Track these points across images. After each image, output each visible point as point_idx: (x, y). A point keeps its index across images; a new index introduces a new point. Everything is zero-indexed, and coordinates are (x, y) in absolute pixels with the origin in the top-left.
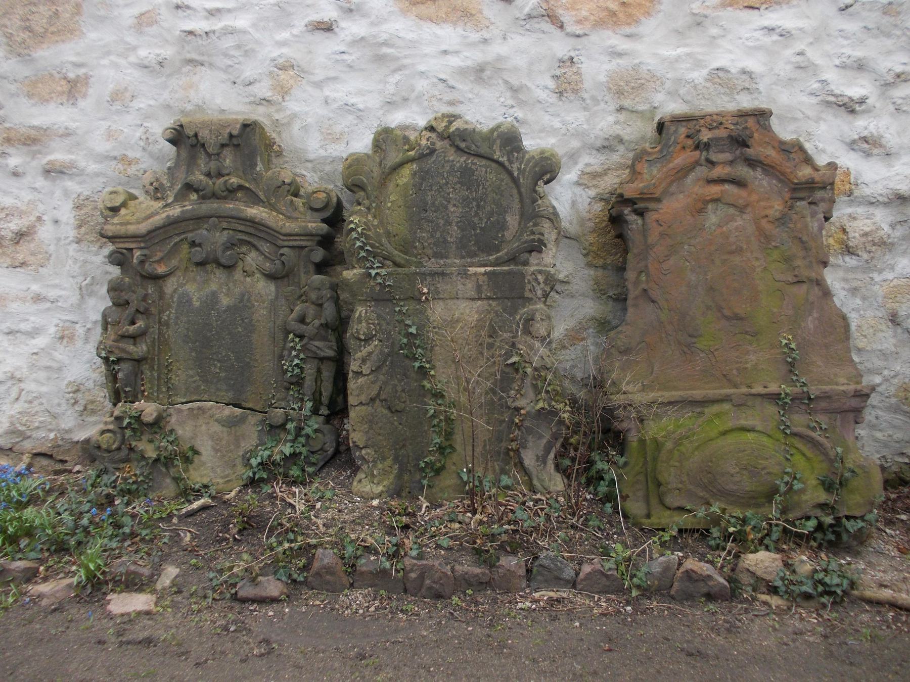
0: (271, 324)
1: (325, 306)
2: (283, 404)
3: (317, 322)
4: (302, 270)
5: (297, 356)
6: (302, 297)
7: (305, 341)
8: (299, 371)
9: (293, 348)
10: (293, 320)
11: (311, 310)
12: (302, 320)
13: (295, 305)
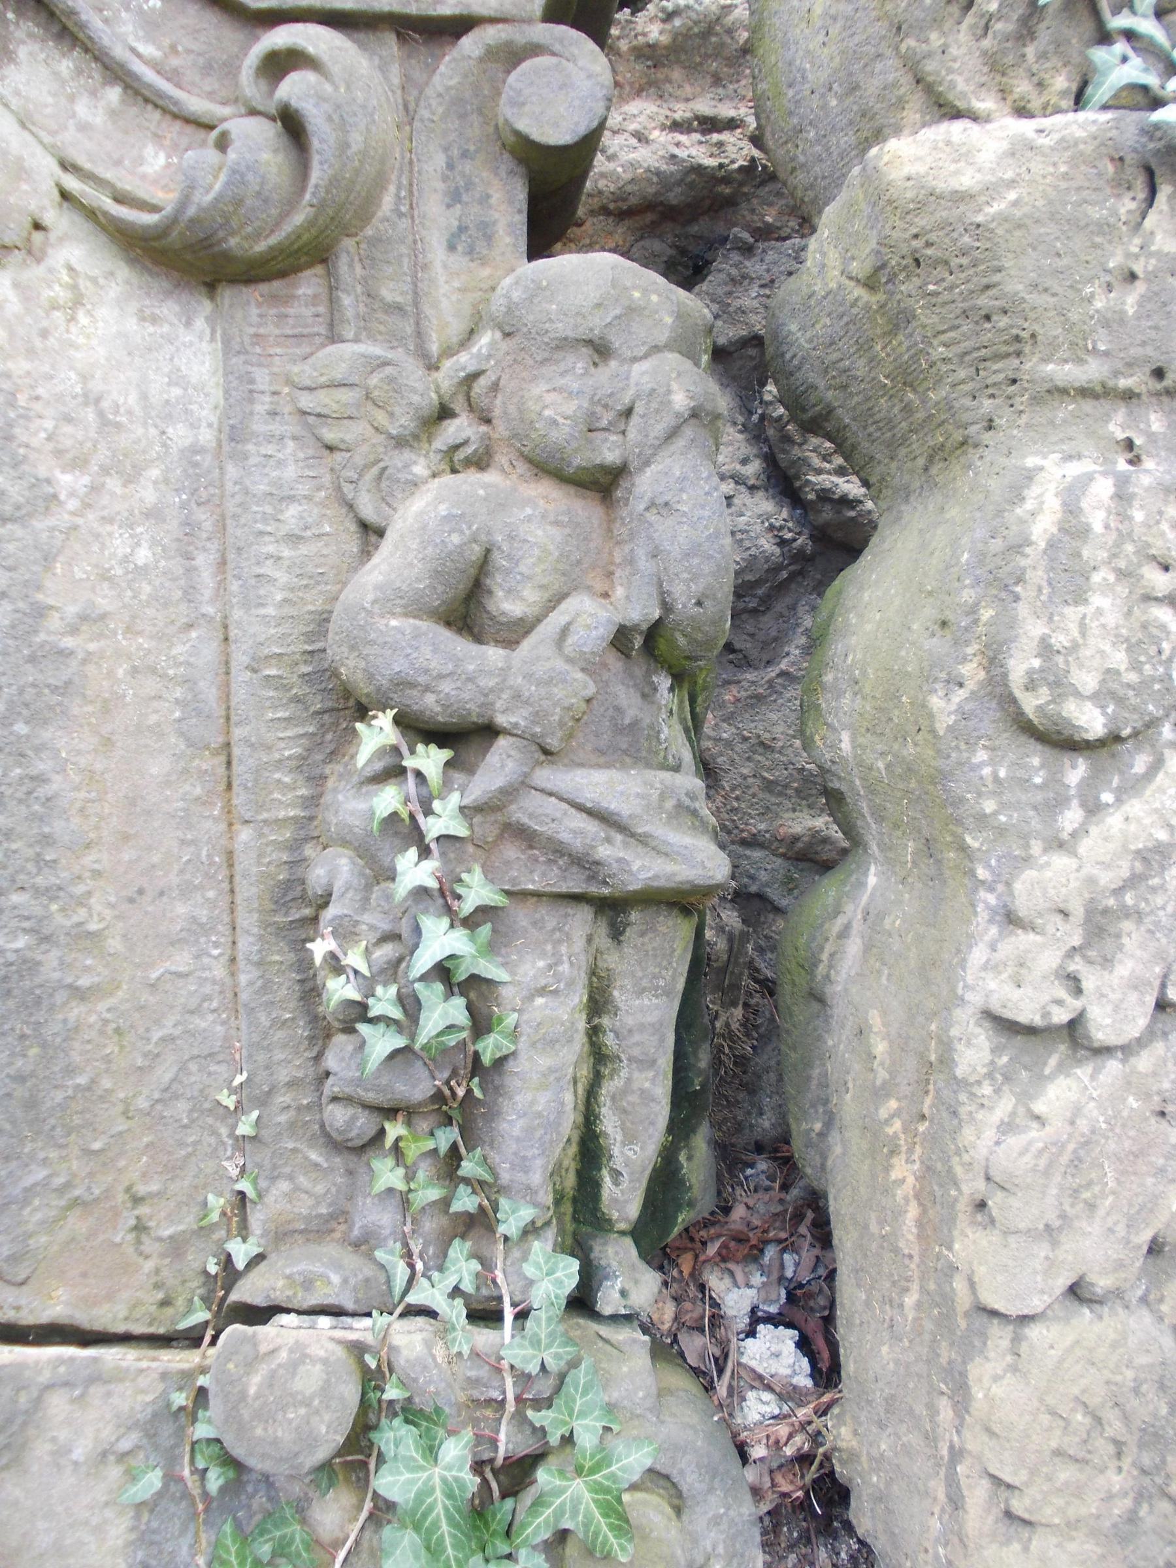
0: (200, 648)
1: (646, 484)
2: (332, 1273)
3: (590, 618)
4: (437, 217)
5: (443, 898)
6: (453, 422)
7: (499, 765)
8: (455, 1011)
9: (406, 831)
10: (390, 600)
11: (534, 524)
12: (466, 607)
13: (391, 487)
